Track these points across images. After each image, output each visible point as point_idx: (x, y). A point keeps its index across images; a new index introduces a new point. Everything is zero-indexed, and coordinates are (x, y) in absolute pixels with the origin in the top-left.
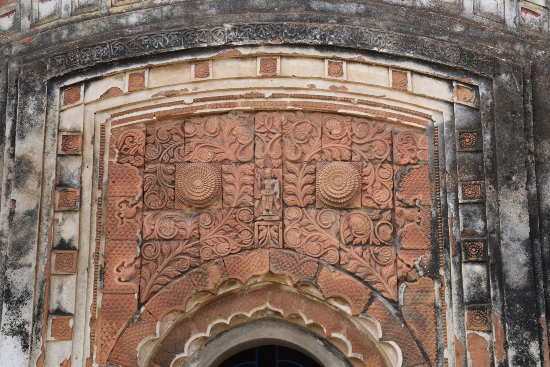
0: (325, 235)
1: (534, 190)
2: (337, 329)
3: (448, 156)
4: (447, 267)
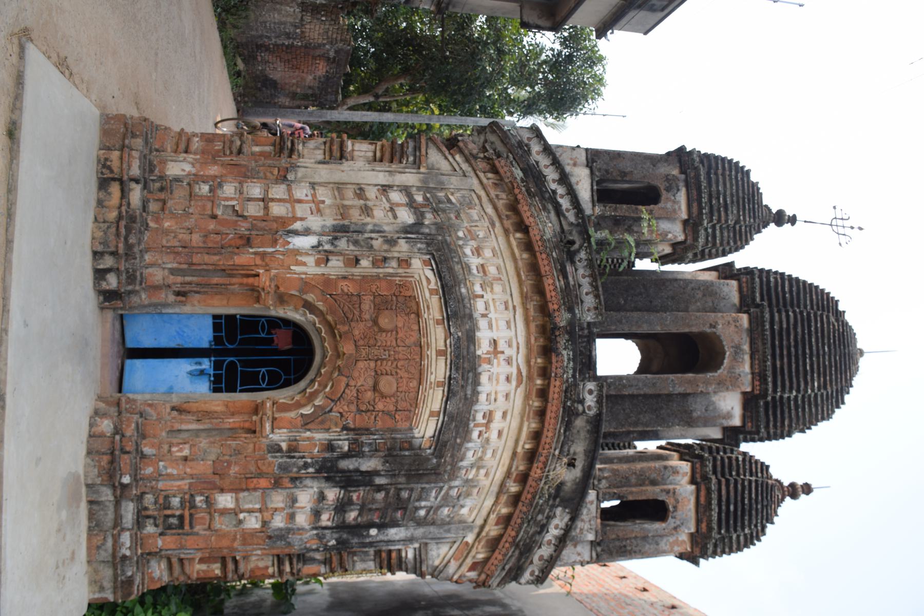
0: (362, 379)
1: (382, 473)
2: (319, 385)
3: (399, 436)
4: (347, 434)
